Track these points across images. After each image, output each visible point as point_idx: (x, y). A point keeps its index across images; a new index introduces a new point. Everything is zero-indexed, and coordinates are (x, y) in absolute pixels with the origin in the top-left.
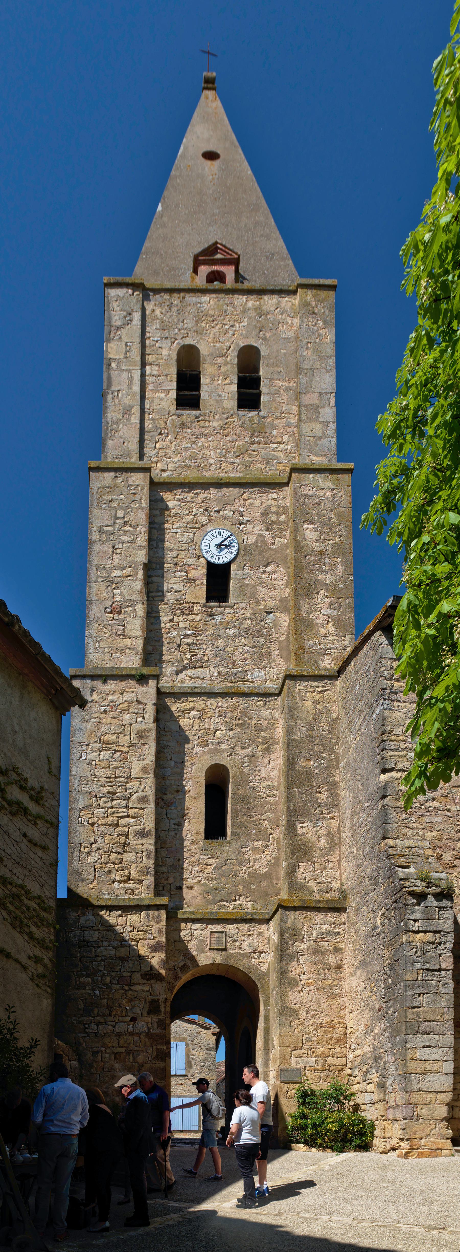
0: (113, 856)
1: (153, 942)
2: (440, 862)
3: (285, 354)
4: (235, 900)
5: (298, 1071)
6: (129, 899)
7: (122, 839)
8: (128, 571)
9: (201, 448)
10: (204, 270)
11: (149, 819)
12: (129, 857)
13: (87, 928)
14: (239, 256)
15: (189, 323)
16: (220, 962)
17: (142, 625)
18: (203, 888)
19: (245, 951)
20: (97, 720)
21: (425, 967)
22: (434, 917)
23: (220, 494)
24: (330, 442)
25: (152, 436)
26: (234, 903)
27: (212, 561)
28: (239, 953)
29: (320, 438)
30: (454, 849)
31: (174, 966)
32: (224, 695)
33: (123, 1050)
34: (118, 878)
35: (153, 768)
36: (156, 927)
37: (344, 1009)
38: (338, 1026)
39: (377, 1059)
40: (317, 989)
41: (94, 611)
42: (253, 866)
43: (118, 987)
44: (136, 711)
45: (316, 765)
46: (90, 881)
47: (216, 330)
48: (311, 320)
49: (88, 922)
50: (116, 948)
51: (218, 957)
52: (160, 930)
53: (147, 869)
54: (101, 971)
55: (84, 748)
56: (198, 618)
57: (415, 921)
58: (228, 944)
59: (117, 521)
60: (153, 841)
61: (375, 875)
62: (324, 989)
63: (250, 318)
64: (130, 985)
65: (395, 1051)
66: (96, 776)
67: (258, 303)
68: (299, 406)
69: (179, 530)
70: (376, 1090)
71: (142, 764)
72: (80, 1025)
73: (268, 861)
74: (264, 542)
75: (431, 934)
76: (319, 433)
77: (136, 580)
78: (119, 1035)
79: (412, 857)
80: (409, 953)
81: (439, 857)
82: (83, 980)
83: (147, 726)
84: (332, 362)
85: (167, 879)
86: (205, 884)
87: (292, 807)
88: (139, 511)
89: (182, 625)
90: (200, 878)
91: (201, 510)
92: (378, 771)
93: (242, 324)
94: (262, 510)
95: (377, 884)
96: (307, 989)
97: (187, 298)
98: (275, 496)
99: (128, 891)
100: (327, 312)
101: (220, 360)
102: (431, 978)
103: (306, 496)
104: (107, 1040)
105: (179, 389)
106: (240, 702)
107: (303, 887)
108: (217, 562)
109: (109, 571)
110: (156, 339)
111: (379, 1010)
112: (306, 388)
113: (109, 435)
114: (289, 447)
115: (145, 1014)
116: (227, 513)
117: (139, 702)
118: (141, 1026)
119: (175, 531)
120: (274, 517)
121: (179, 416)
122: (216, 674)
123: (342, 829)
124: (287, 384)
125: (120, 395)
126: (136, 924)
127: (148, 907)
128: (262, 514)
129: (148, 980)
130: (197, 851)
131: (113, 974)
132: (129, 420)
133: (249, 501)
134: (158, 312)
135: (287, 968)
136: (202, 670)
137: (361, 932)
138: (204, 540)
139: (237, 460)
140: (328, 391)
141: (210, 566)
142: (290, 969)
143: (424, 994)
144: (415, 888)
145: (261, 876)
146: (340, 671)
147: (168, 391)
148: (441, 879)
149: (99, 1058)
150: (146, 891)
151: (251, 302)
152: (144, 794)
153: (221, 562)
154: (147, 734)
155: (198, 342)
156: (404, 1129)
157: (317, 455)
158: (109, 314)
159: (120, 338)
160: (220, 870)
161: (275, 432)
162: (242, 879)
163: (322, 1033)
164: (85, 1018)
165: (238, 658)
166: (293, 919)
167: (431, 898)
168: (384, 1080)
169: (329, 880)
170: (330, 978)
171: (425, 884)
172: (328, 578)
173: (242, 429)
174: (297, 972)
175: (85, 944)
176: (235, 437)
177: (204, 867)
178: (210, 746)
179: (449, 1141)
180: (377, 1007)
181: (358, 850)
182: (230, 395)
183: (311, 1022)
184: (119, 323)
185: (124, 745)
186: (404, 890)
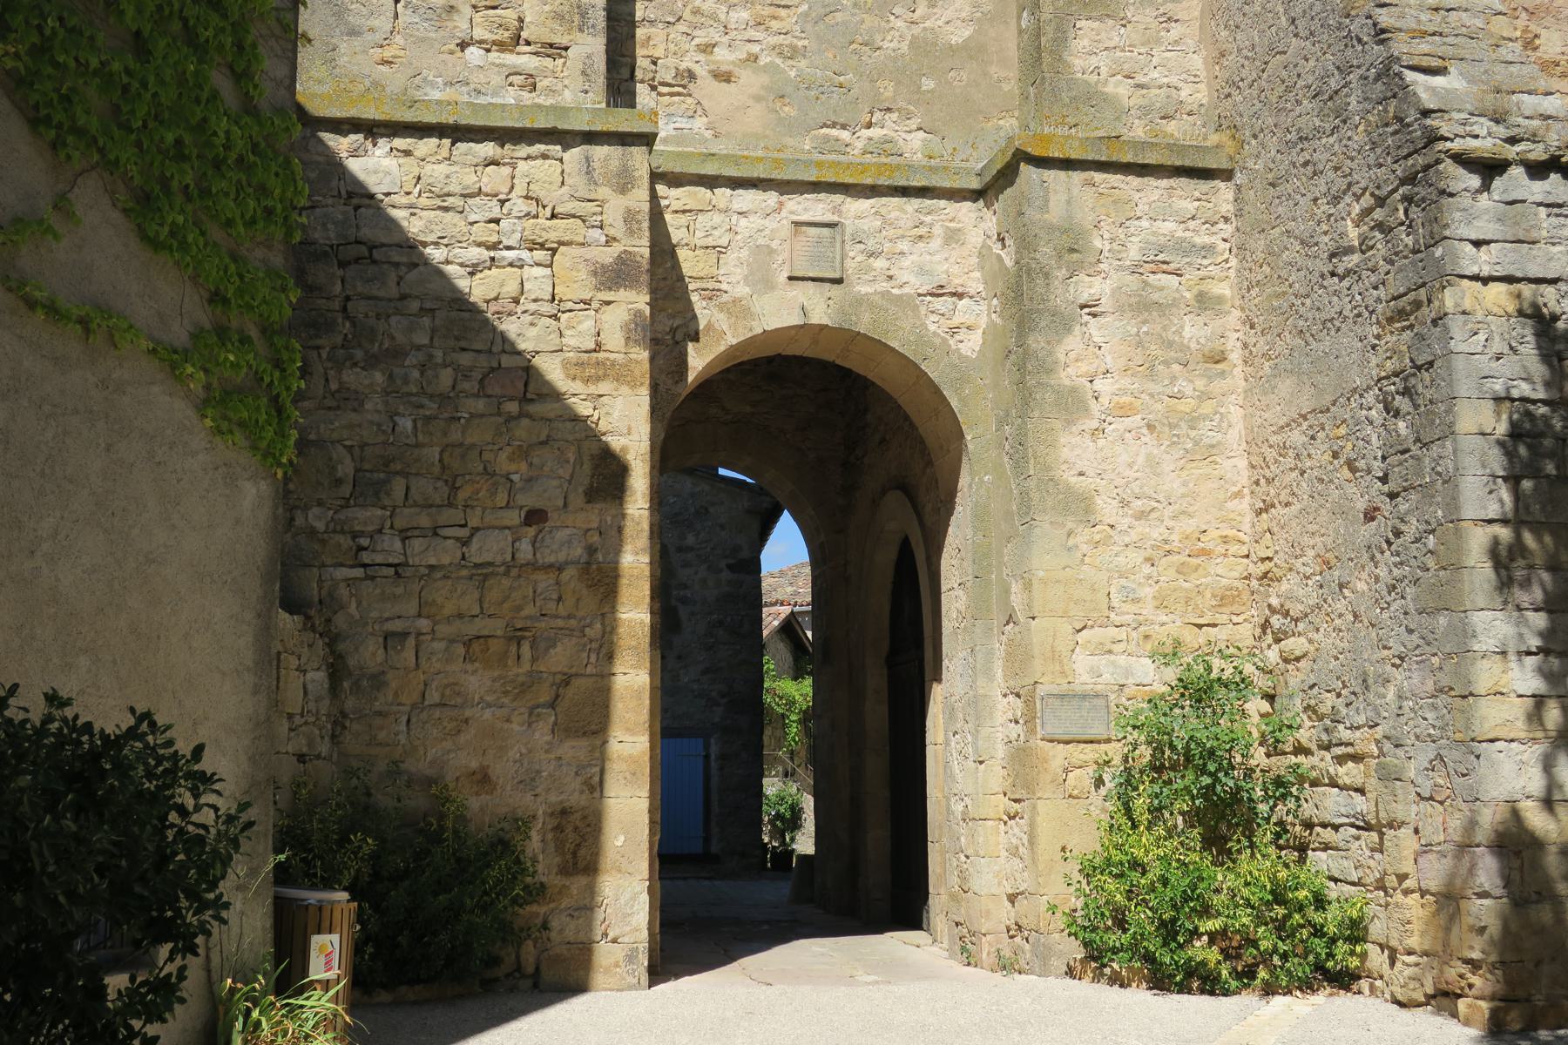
1: (607, 256)
2: (1533, 56)
4: (869, 125)
5: (1101, 702)
6: (520, 107)
16: (825, 321)
18: (765, 79)
19: (906, 290)
22: (1534, 235)
26: (866, 133)
28: (885, 295)
31: (673, 331)
34: (478, 33)
40: (1150, 427)
42: (925, 18)
43: (480, 405)
46: (379, 37)
51: (819, 308)
52: (630, 217)
54: (419, 348)
57: (1478, 244)
58: (849, 263)
61: (1334, 84)
62: (1171, 426)
72: (341, 538)
78: (483, 574)
79: (1451, 40)
80: (1462, 347)
81: (1530, 44)
82: (351, 377)
86: (770, 69)
90: (755, 48)
96: (1120, 425)
99: (517, 79)
107: (1092, 98)
111: (1370, 515)
115: (577, 500)
126: (555, 196)
127: (591, 138)
131: (465, 359)
135: (1051, 353)
142: (1062, 357)
144: (1472, 143)
145: (953, 50)
150: (579, 83)
160: (821, 25)
162: (895, 59)
163: (1172, 573)
166: (1064, 197)
167: (1517, 172)
169: (1173, 80)
170: (1188, 391)
171: (1501, 131)
174: (1084, 367)
177: (768, 11)
180: (1361, 505)
183: (1134, 536)
186: (1441, 146)
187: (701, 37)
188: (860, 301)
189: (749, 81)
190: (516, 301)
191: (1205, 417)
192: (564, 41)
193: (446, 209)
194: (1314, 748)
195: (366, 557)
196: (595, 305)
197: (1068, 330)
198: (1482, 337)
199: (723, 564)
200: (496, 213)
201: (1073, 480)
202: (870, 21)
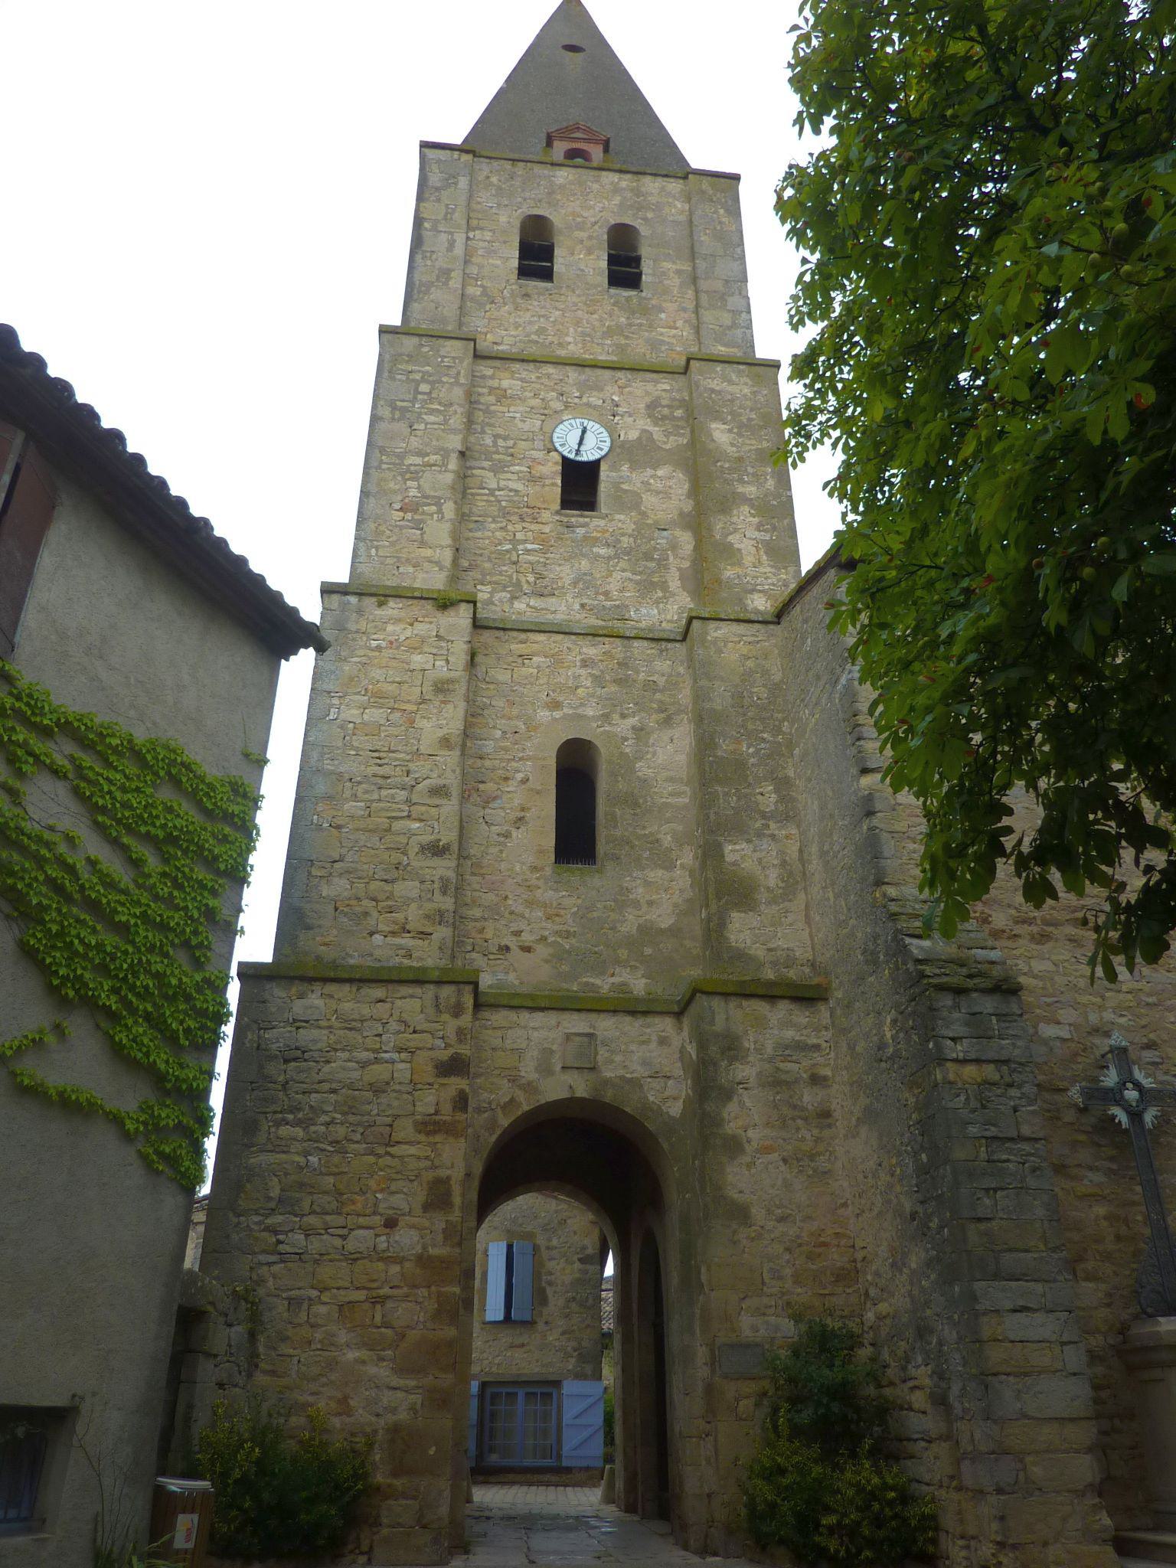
0: (374, 886)
1: (444, 1055)
2: (986, 928)
7: (396, 857)
8: (433, 458)
12: (407, 888)
13: (307, 1022)
16: (585, 1095)
18: (551, 950)
20: (364, 659)
21: (988, 1134)
22: (990, 1033)
23: (583, 377)
28: (622, 1078)
29: (730, 328)
30: (1009, 906)
32: (593, 634)
33: (360, 1295)
37: (845, 1205)
38: (835, 1242)
39: (923, 1331)
40: (785, 1161)
44: (434, 651)
45: (751, 750)
49: (309, 1012)
50: (364, 1065)
53: (441, 913)
55: (336, 701)
57: (953, 1039)
59: (420, 397)
62: (798, 1160)
65: (956, 1317)
66: (353, 748)
68: (697, 292)
70: (929, 1408)
71: (440, 733)
73: (676, 905)
75: (992, 1066)
76: (728, 322)
78: (353, 1259)
80: (950, 1105)
82: (285, 1131)
83: (452, 674)
85: (482, 931)
87: (712, 817)
92: (854, 771)
94: (648, 400)
95: (876, 962)
99: (399, 952)
101: (583, 235)
102: (1005, 1157)
103: (713, 391)
104: (326, 1272)
105: (520, 258)
106: (616, 647)
107: (740, 956)
109: (401, 457)
115: (418, 1211)
118: (407, 1239)
120: (666, 411)
122: (577, 607)
123: (805, 856)
126: (418, 1020)
129: (428, 1134)
130: (541, 883)
132: (446, 284)
136: (553, 600)
137: (859, 1049)
142: (725, 1115)
143: (995, 1190)
145: (662, 932)
146: (779, 616)
148: (993, 963)
149: (303, 1316)
152: (441, 782)
156: (1002, 1518)
157: (724, 345)
161: (663, 316)
164: (279, 1219)
165: (613, 586)
168: (943, 1385)
169: (791, 945)
170: (808, 1137)
172: (751, 490)
175: (295, 1055)
178: (565, 710)
179: (1110, 1549)
181: (837, 896)
185: (409, 701)
187: (514, 927)
188: (607, 1082)
189: (542, 951)
190: (388, 1083)
191: (819, 1154)
192: (430, 930)
193: (350, 1029)
194: (897, 1382)
195: (281, 1248)
196: (436, 1086)
197: (729, 1098)
198: (962, 1098)
199: (575, 1258)
200: (380, 1030)
201: (736, 1196)
202: (613, 916)
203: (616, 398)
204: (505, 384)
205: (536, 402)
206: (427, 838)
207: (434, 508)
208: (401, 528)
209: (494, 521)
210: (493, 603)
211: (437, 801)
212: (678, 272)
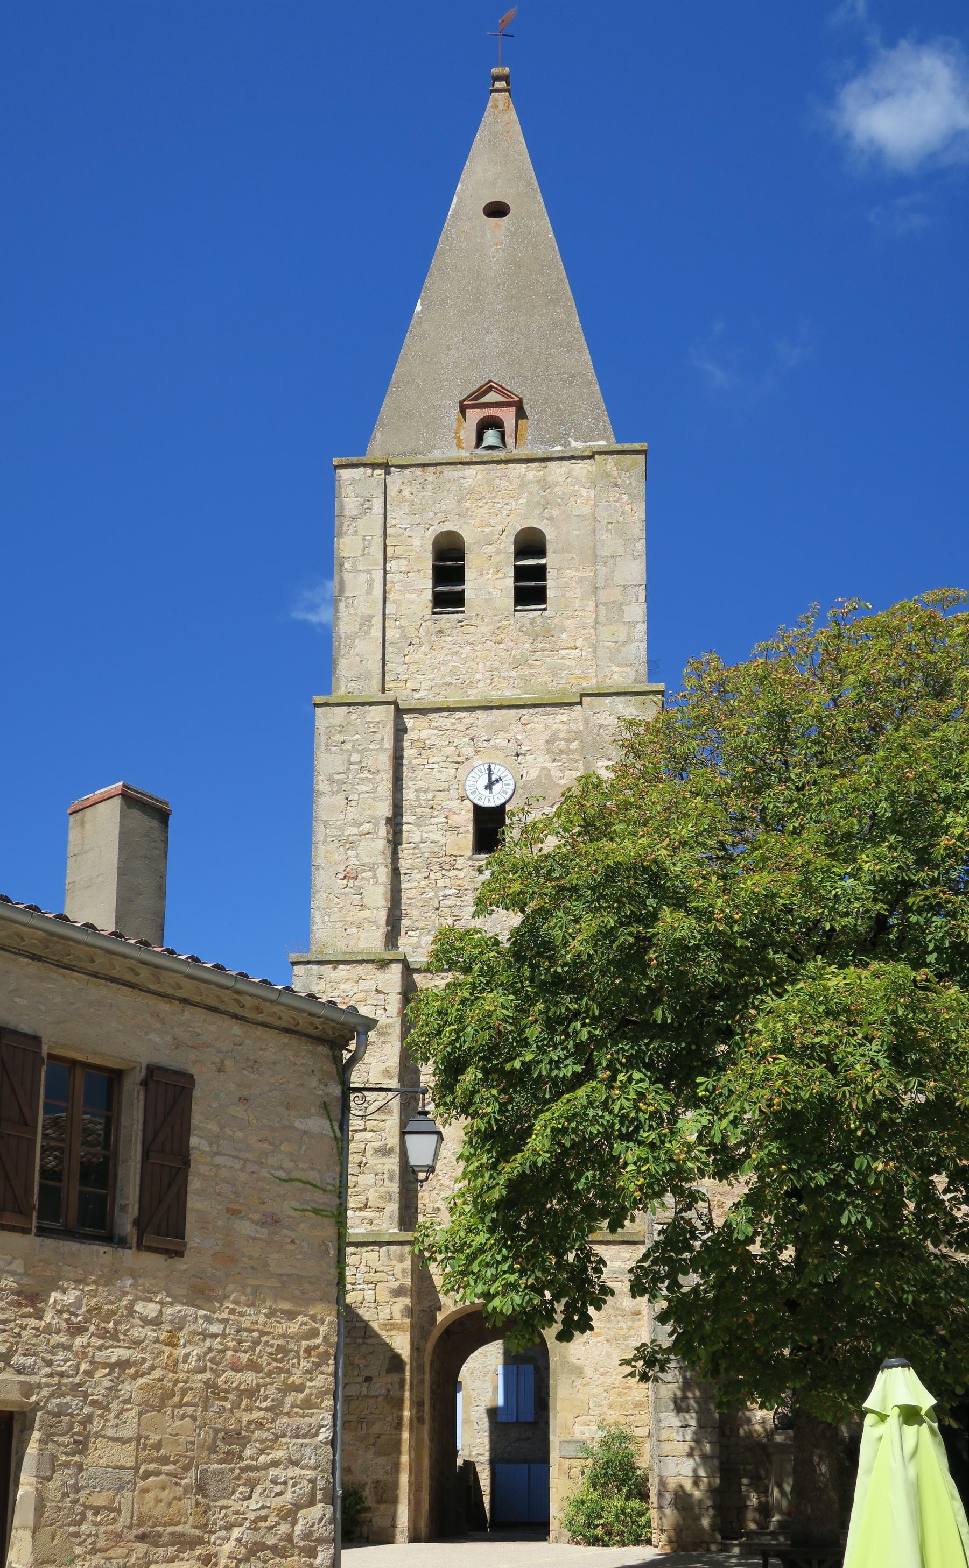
1: (395, 1285)
3: (578, 536)
8: (366, 828)
9: (466, 660)
10: (475, 416)
11: (392, 1133)
14: (521, 400)
15: (449, 504)
17: (386, 893)
23: (491, 718)
24: (638, 649)
25: (399, 648)
27: (480, 803)
29: (624, 644)
35: (397, 1071)
36: (399, 1267)
40: (608, 1341)
41: (322, 878)
47: (485, 510)
48: (612, 494)
56: (461, 874)
59: (352, 767)
60: (397, 1160)
63: (530, 493)
64: (364, 1338)
67: (541, 473)
69: (435, 766)
71: (383, 1067)
74: (548, 776)
77: (377, 838)
84: (641, 546)
88: (381, 754)
89: (440, 884)
91: (466, 740)
93: (520, 501)
94: (546, 736)
97: (445, 473)
98: (564, 718)
100: (634, 483)
101: (491, 549)
103: (601, 726)
108: (487, 805)
109: (341, 828)
110: (404, 526)
112: (605, 581)
113: (342, 652)
114: (584, 653)
115: (383, 1373)
116: (501, 741)
117: (378, 991)
119: (430, 766)
120: (563, 745)
121: (435, 621)
124: (580, 574)
125: (356, 602)
126: (375, 1264)
128: (547, 742)
132: (368, 633)
133: (529, 726)
134: (406, 493)
138: (470, 778)
139: (514, 674)
140: (635, 583)
141: (479, 811)
147: (422, 590)
151: (532, 472)
153: (492, 805)
154: (389, 1031)
155: (460, 528)
158: (341, 502)
159: (356, 531)
161: (564, 636)
170: (624, 1326)
173: (521, 633)
176: (512, 644)
182: (504, 592)
183: (600, 1382)
184: (354, 512)
200: (354, 1272)
203: (519, 737)
204: (424, 734)
205: (450, 750)
206: (378, 1144)
207: (370, 873)
208: (346, 895)
209: (419, 872)
210: (421, 947)
211: (383, 1117)
212: (581, 580)
